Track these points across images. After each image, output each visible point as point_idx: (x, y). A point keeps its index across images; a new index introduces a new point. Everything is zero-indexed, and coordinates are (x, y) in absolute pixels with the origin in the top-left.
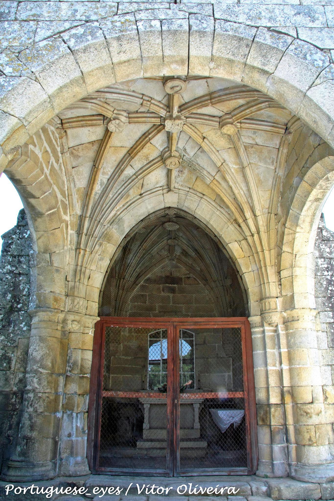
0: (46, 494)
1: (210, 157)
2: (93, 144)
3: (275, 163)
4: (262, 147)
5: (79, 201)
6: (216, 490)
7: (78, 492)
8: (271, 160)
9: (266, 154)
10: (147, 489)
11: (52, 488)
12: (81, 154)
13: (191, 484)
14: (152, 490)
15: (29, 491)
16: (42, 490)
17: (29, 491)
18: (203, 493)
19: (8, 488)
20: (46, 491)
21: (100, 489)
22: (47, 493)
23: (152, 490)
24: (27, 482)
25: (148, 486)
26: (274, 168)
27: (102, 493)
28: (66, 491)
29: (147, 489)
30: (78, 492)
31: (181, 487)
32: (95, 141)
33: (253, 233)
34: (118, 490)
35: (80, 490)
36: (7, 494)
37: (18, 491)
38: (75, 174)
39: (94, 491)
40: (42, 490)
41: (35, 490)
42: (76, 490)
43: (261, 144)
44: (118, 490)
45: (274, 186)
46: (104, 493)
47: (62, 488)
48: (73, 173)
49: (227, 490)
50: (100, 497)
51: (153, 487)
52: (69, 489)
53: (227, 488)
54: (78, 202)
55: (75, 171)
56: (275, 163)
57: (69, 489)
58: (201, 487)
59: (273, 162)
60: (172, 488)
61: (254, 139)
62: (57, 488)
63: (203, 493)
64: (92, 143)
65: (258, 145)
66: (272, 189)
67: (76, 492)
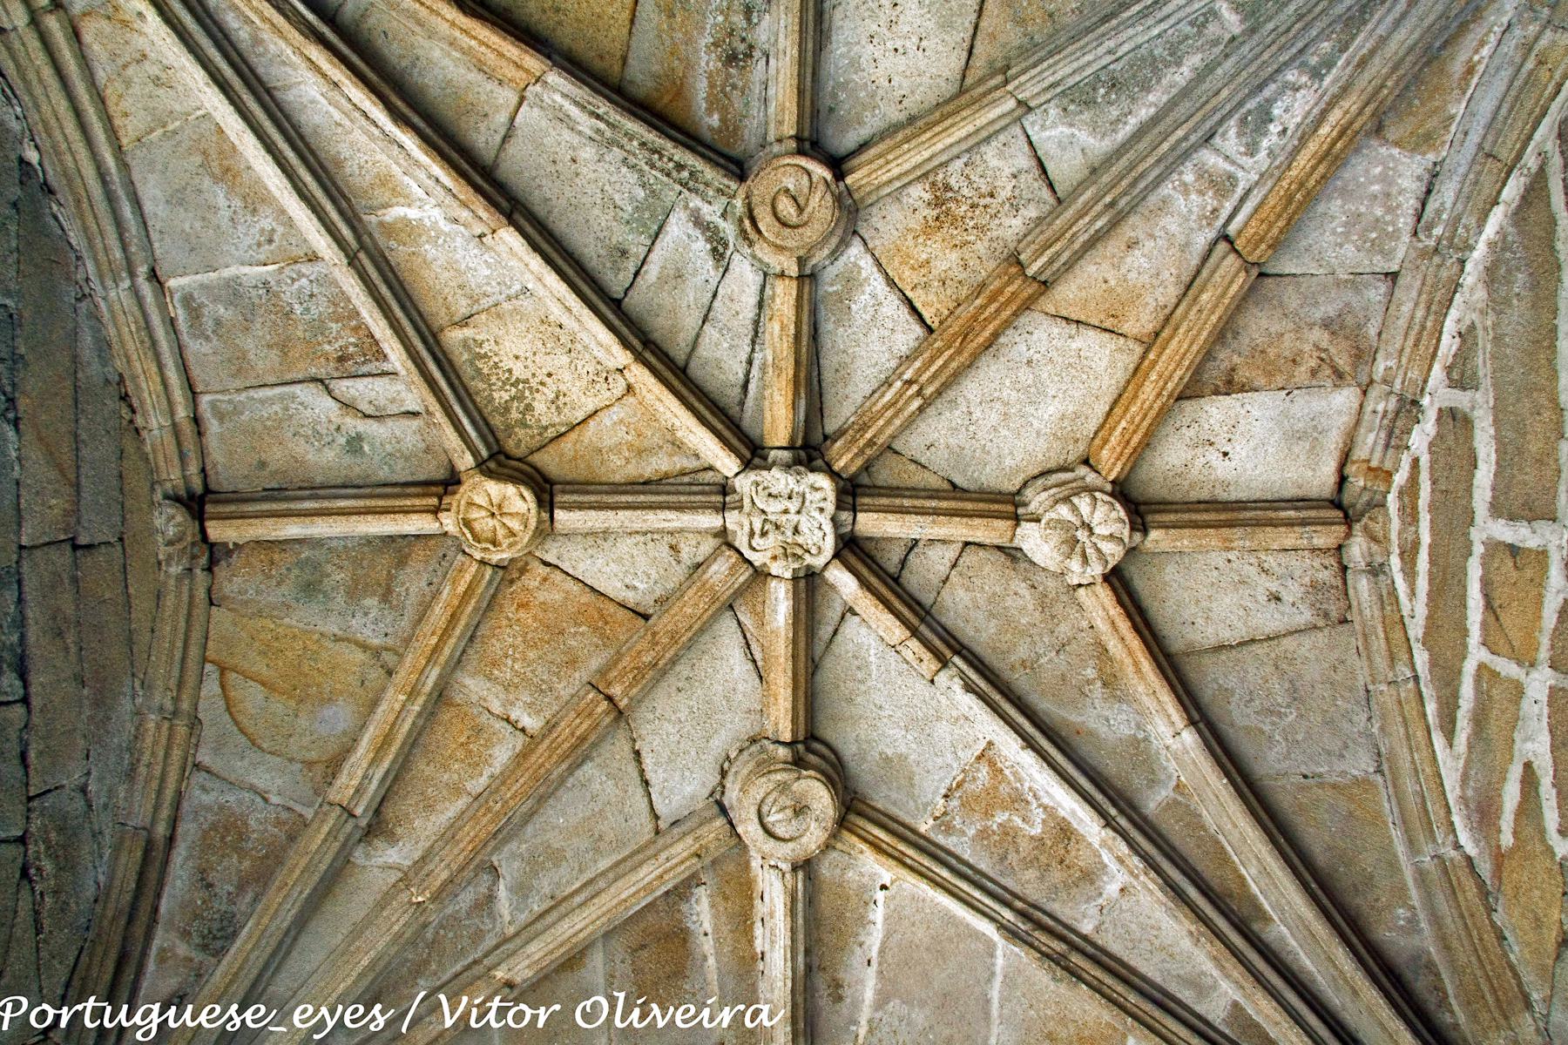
0: (136, 1028)
1: (552, 440)
2: (1230, 382)
3: (181, 315)
4: (288, 377)
5: (1457, 67)
6: (706, 1013)
7: (243, 1021)
8: (209, 324)
9: (249, 343)
10: (475, 1011)
11: (156, 1007)
12: (1319, 336)
13: (621, 996)
14: (492, 1015)
15: (78, 1016)
16: (123, 1015)
17: (78, 1016)
18: (661, 1024)
19: (10, 1006)
20: (137, 1019)
21: (316, 1011)
22: (140, 1023)
23: (492, 1015)
24: (174, 828)
25: (477, 1002)
26: (172, 283)
27: (322, 1024)
28: (203, 1018)
29: (475, 1011)
30: (243, 1021)
31: (589, 1003)
32: (1217, 392)
33: (1139, 350)
34: (378, 1015)
35: (248, 1015)
36: (5, 1027)
37: (42, 1016)
38: (1395, 235)
39: (296, 1017)
40: (123, 1015)
41: (98, 1014)
42: (235, 1015)
43: (297, 389)
44: (378, 1015)
45: (121, 191)
46: (330, 1024)
47: (190, 1007)
48: (1402, 248)
49: (743, 1013)
50: (316, 1037)
51: (496, 1003)
52: (212, 1011)
53: (742, 1007)
54: (1470, 71)
55: (1387, 255)
56: (181, 315)
57: (212, 1011)
58: (654, 1006)
59: (194, 312)
60: (557, 1007)
61: (347, 406)
62: (174, 1008)
63: (661, 1024)
64: (1230, 386)
65: (314, 380)
66: (124, 166)
67: (237, 1020)
